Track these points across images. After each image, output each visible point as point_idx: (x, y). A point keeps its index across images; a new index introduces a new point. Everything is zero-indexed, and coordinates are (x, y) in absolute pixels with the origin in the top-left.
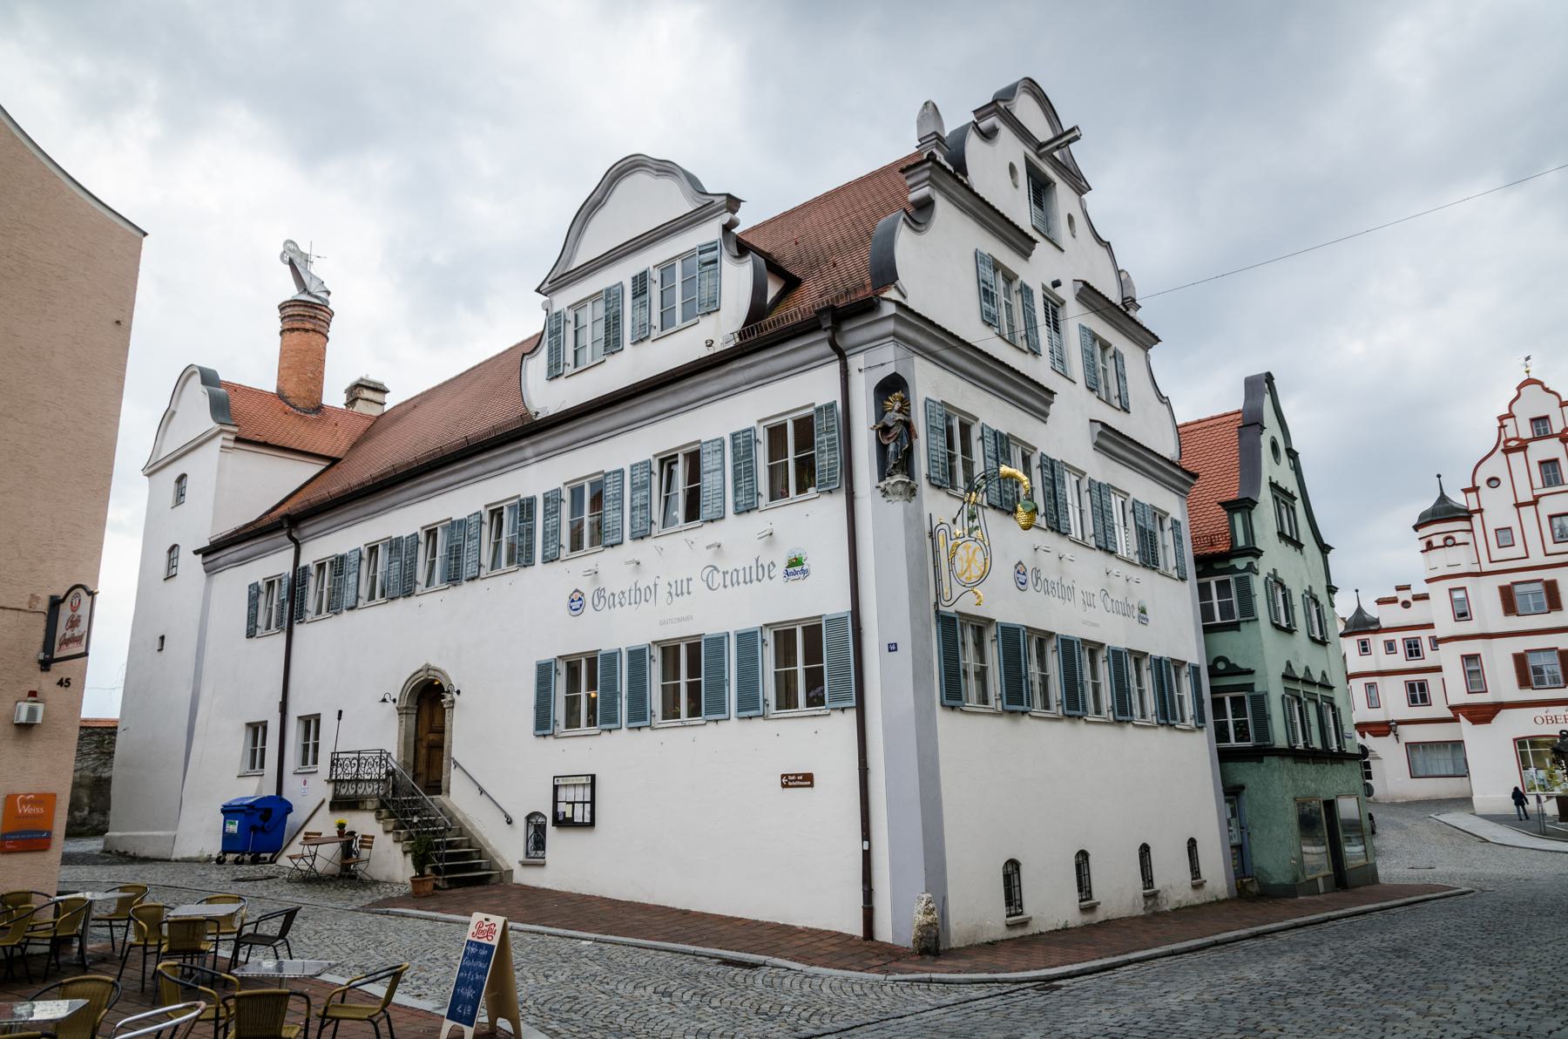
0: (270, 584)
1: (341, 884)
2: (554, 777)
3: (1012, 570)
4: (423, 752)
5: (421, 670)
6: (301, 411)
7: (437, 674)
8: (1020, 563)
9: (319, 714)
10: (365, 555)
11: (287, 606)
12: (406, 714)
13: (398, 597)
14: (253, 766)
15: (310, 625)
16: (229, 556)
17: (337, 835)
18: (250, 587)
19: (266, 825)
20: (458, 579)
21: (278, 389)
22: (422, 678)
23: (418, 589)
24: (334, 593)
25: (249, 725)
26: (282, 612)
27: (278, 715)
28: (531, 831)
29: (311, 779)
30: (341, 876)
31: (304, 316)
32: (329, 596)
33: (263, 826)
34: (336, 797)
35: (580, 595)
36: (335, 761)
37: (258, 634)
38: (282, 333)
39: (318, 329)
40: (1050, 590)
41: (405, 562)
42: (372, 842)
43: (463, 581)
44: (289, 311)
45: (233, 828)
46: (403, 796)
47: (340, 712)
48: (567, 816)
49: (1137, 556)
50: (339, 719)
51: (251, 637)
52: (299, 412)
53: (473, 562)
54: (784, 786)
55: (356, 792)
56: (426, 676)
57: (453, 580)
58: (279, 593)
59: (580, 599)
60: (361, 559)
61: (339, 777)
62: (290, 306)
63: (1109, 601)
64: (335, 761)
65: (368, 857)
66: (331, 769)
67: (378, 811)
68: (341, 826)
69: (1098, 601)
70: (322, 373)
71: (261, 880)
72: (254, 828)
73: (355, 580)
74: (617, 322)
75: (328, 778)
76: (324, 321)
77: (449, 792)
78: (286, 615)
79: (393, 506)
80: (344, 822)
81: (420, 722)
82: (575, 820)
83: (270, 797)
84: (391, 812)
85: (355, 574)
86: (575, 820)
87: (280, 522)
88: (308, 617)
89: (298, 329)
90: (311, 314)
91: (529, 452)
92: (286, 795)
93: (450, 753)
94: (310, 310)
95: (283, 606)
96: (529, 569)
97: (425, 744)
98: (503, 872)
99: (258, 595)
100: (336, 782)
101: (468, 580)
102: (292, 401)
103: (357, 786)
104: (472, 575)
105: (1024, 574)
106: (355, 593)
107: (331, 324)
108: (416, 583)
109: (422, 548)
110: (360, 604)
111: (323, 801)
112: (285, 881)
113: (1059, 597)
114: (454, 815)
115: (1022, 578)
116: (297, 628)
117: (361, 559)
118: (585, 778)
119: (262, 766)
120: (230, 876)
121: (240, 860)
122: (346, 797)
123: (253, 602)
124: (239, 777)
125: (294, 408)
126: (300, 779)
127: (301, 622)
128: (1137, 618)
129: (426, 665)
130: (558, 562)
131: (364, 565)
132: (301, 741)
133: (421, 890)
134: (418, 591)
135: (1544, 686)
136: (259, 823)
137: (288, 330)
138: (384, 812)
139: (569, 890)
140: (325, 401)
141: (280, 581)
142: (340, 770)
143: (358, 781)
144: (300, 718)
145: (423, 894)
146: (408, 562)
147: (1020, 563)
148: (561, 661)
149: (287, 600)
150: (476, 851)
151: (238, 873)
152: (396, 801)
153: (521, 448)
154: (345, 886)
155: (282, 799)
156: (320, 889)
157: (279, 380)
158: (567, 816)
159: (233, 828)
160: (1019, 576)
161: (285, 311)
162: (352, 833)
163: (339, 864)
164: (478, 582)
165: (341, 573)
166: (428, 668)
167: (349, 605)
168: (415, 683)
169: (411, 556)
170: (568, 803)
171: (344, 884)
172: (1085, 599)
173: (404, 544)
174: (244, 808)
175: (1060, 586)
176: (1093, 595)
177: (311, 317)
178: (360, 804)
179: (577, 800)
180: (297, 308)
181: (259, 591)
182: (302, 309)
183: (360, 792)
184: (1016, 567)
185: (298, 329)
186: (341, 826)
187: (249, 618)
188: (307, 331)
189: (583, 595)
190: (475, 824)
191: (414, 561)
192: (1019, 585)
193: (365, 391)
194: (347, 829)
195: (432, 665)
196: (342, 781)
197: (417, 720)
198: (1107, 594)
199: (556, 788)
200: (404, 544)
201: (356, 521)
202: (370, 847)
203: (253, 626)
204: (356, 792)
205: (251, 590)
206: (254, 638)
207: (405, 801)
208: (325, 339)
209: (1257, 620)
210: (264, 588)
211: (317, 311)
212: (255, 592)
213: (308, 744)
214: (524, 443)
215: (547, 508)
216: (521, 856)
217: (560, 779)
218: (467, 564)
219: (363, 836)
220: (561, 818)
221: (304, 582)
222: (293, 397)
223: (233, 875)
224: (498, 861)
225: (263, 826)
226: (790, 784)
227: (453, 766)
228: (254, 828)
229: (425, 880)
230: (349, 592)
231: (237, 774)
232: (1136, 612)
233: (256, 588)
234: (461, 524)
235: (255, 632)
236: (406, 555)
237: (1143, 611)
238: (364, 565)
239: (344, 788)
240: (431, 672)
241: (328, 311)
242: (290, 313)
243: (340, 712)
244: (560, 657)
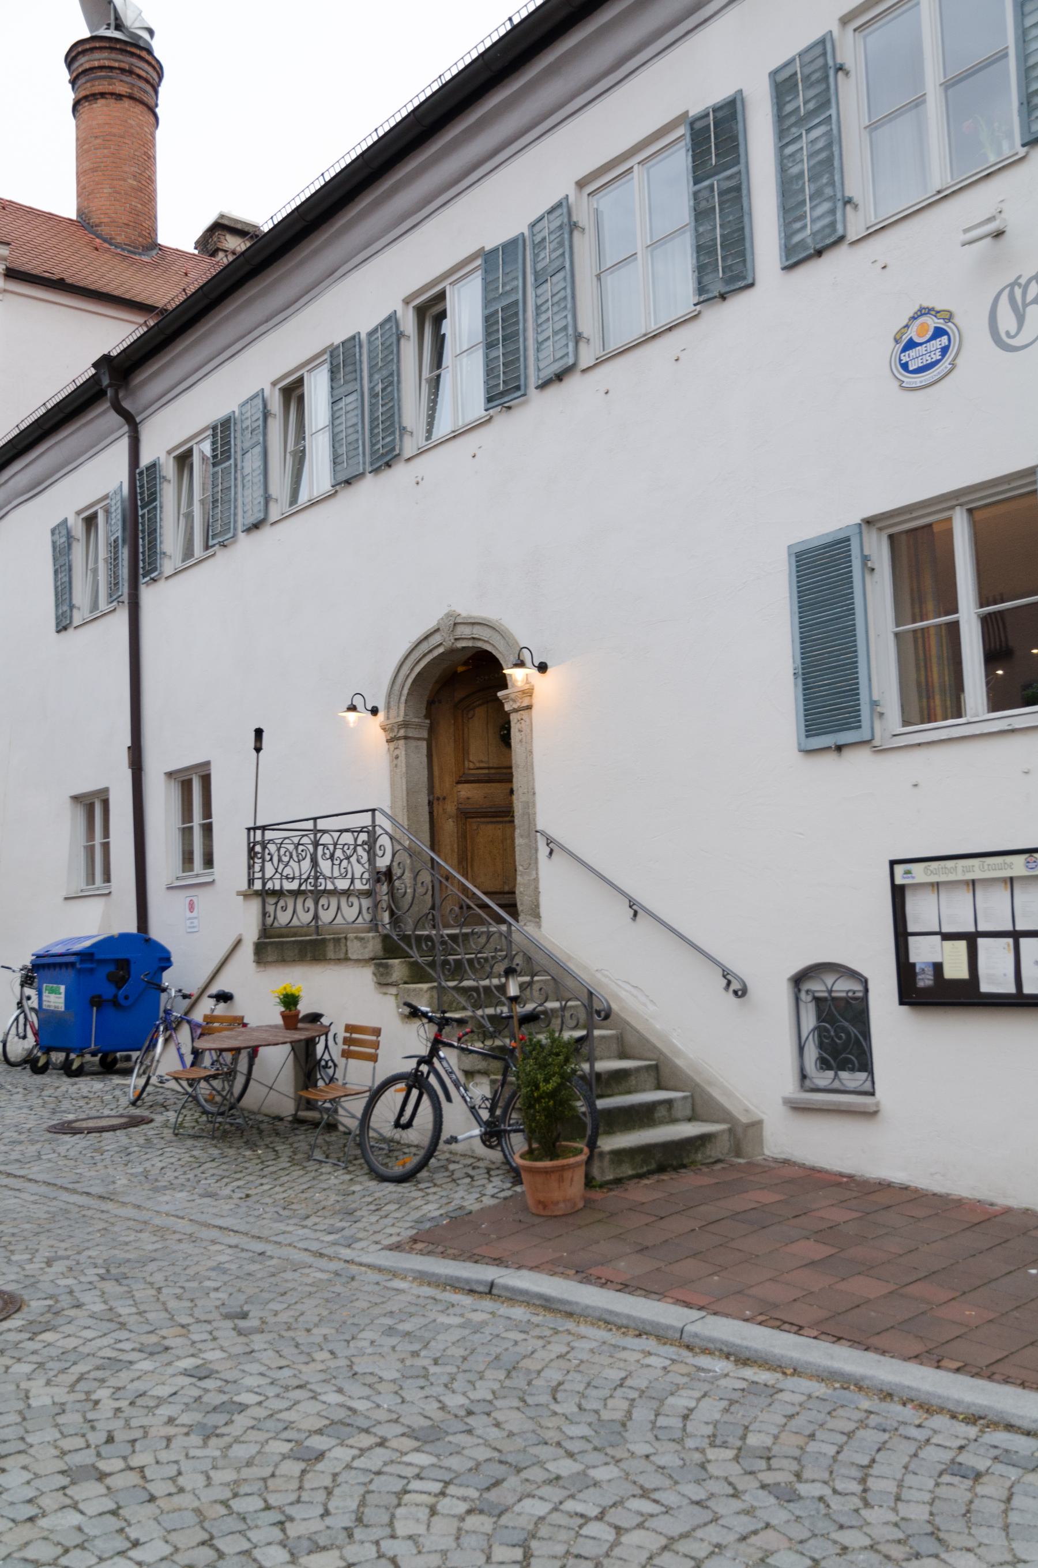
0: (90, 522)
1: (304, 1146)
2: (893, 863)
4: (449, 827)
5: (437, 630)
6: (123, 249)
7: (478, 632)
9: (207, 764)
10: (276, 404)
11: (125, 553)
12: (406, 738)
13: (361, 476)
14: (91, 878)
15: (171, 581)
16: (11, 483)
17: (279, 1021)
18: (53, 532)
19: (121, 993)
20: (518, 388)
21: (80, 212)
22: (441, 650)
23: (409, 447)
24: (215, 502)
25: (76, 799)
26: (116, 566)
27: (128, 774)
28: (809, 1021)
29: (202, 897)
30: (298, 1121)
31: (111, 68)
32: (205, 513)
33: (116, 996)
34: (266, 931)
35: (932, 323)
36: (258, 848)
37: (77, 620)
38: (76, 105)
39: (138, 94)
41: (371, 389)
42: (376, 1045)
43: (532, 391)
44: (84, 62)
45: (56, 999)
46: (447, 926)
47: (259, 733)
48: (949, 974)
50: (258, 749)
51: (65, 628)
52: (119, 251)
53: (555, 333)
55: (316, 917)
56: (448, 644)
57: (502, 394)
58: (110, 529)
59: (939, 333)
60: (266, 415)
61: (269, 885)
62: (84, 52)
64: (258, 848)
65: (773, 1467)
66: (250, 867)
67: (380, 964)
68: (290, 1001)
70: (151, 180)
71: (113, 1129)
72: (97, 1002)
73: (258, 463)
74: (512, 347)
75: (244, 886)
76: (147, 81)
77: (538, 916)
78: (124, 572)
79: (331, 275)
80: (294, 991)
81: (435, 759)
82: (985, 988)
83: (124, 937)
84: (415, 964)
85: (258, 449)
86: (985, 988)
87: (94, 380)
88: (168, 567)
89: (103, 95)
90: (123, 65)
92: (157, 932)
93: (530, 818)
94: (120, 57)
95: (116, 553)
96: (739, 303)
97: (451, 808)
98: (739, 1130)
99: (70, 546)
100: (264, 894)
101: (543, 386)
102: (104, 230)
103: (316, 903)
104: (556, 367)
106: (261, 492)
107: (161, 90)
108: (403, 430)
109: (409, 350)
110: (274, 514)
111: (238, 943)
112: (168, 1133)
116: (148, 595)
117: (266, 415)
119: (107, 878)
120: (45, 1114)
121: (75, 1066)
122: (289, 930)
123: (61, 561)
124: (66, 899)
125: (111, 244)
126: (181, 899)
127: (154, 580)
129: (448, 615)
130: (843, 250)
131: (275, 426)
132: (176, 821)
133: (557, 1195)
134: (409, 449)
136: (108, 991)
137: (86, 98)
138: (398, 967)
139: (978, 1195)
140: (163, 239)
141: (107, 512)
142: (269, 870)
143: (318, 894)
144: (170, 775)
145: (561, 1208)
146: (380, 387)
148: (874, 534)
149: (124, 541)
150: (648, 1068)
151: (66, 1104)
152: (429, 938)
154: (318, 1155)
155: (148, 941)
156: (253, 1166)
157: (79, 195)
158: (949, 974)
159: (56, 999)
161: (76, 64)
162: (315, 1018)
163: (292, 1095)
164: (574, 383)
165: (226, 455)
166: (456, 623)
167: (251, 520)
168: (423, 664)
169: (385, 373)
170: (947, 937)
171: (313, 1147)
173: (365, 350)
174: (72, 959)
177: (123, 70)
178: (330, 947)
179: (982, 928)
180: (97, 55)
181: (69, 537)
182: (105, 54)
183: (326, 917)
185: (103, 95)
186: (290, 1001)
187: (56, 595)
188: (119, 97)
189: (949, 317)
190: (623, 994)
191: (391, 382)
193: (229, 237)
194: (304, 1008)
195: (464, 614)
196: (279, 894)
197: (430, 756)
199: (898, 894)
200: (365, 350)
201: (247, 338)
202: (374, 1058)
203: (66, 608)
204: (316, 917)
205: (57, 537)
206: (71, 631)
207: (453, 938)
208: (152, 119)
210: (78, 529)
211: (134, 61)
212: (63, 539)
213: (191, 828)
215: (789, 108)
216: (788, 1086)
217: (917, 868)
218: (539, 345)
219: (349, 1028)
220: (925, 980)
221: (153, 497)
222: (106, 224)
223: (54, 1112)
224: (716, 1093)
225: (116, 996)
227: (543, 850)
228: (97, 1002)
229: (563, 1168)
230: (247, 492)
231: (64, 894)
233: (64, 532)
234: (511, 248)
235: (71, 617)
236: (371, 376)
238: (275, 426)
239: (284, 909)
240: (465, 631)
241: (154, 62)
242: (87, 66)
243: (259, 733)
244: (869, 522)
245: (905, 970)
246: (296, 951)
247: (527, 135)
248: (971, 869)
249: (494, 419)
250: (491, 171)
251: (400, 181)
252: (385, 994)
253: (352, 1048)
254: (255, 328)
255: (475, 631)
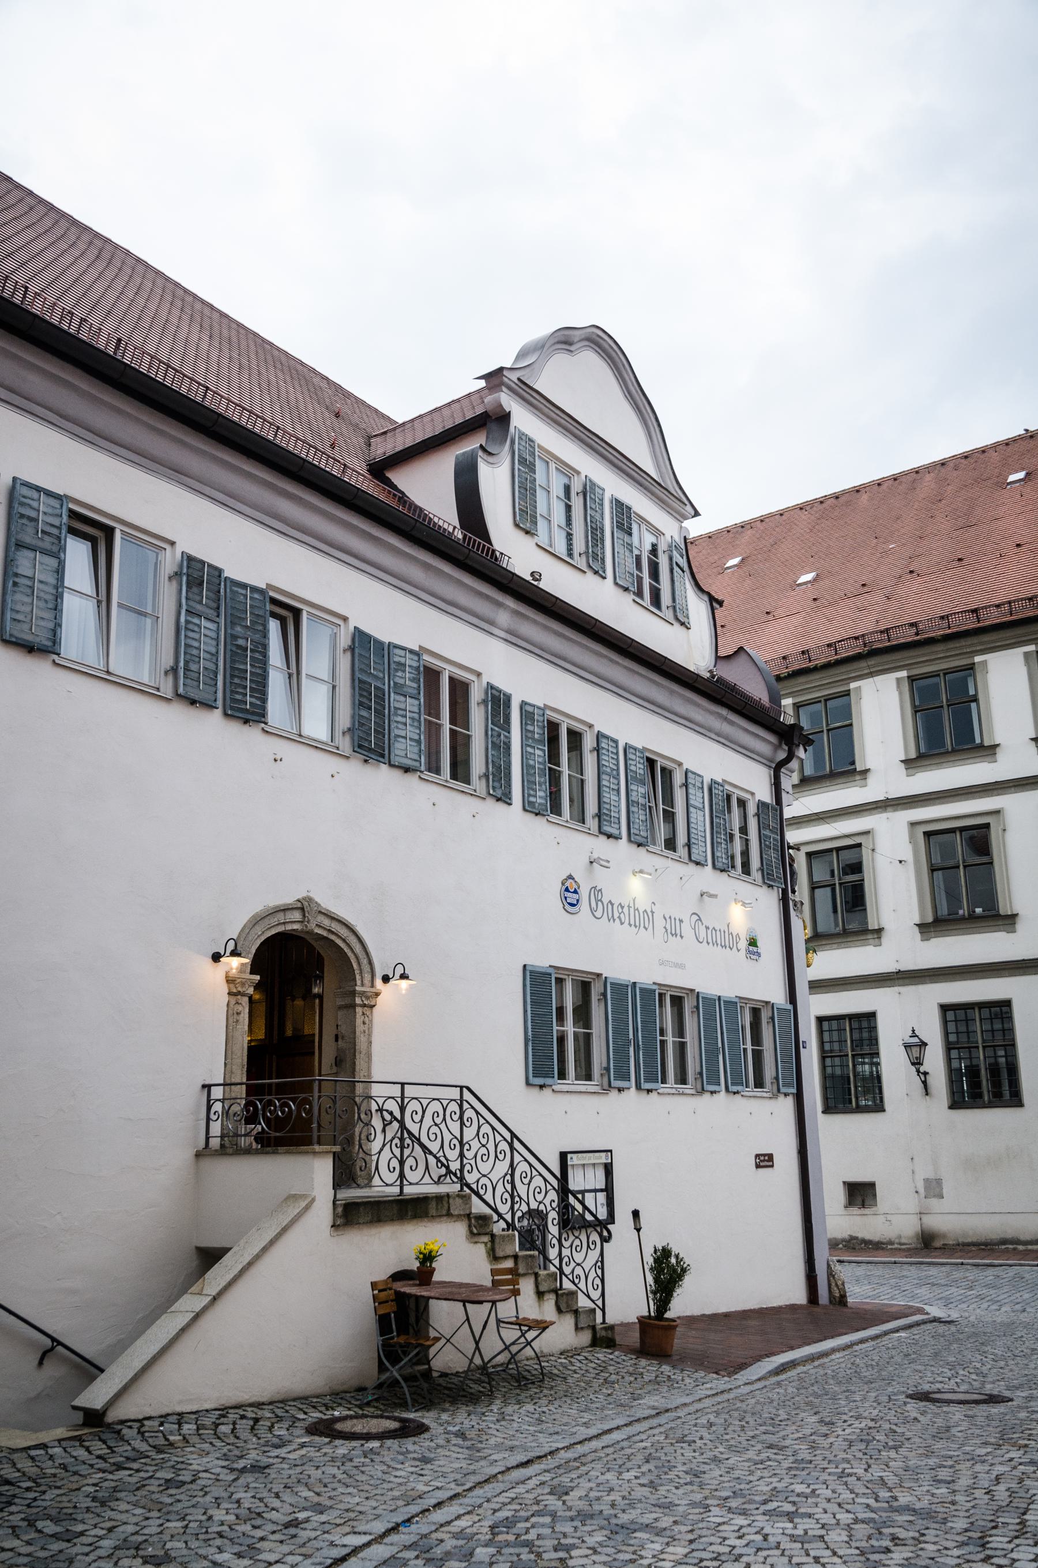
2: (611, 1151)
3: (557, 887)
8: (570, 877)
40: (616, 915)
49: (348, 738)
54: (758, 1166)
63: (703, 929)
69: (687, 929)
91: (503, 618)
105: (575, 892)
113: (630, 925)
114: (488, 1253)
115: (572, 898)
118: (603, 1155)
128: (743, 952)
135: (531, 1075)
147: (570, 877)
153: (499, 605)
160: (568, 894)
172: (668, 927)
175: (632, 910)
176: (681, 921)
184: (563, 884)
192: (567, 907)
198: (700, 919)
209: (865, 910)
214: (510, 602)
226: (762, 1164)
232: (743, 944)
237: (753, 943)
245: (564, 1208)
246: (395, 1211)
247: (376, 570)
248: (590, 1159)
249: (351, 760)
250: (358, 568)
251: (301, 498)
252: (476, 1243)
253: (512, 1287)
254: (38, 404)
255: (333, 925)
